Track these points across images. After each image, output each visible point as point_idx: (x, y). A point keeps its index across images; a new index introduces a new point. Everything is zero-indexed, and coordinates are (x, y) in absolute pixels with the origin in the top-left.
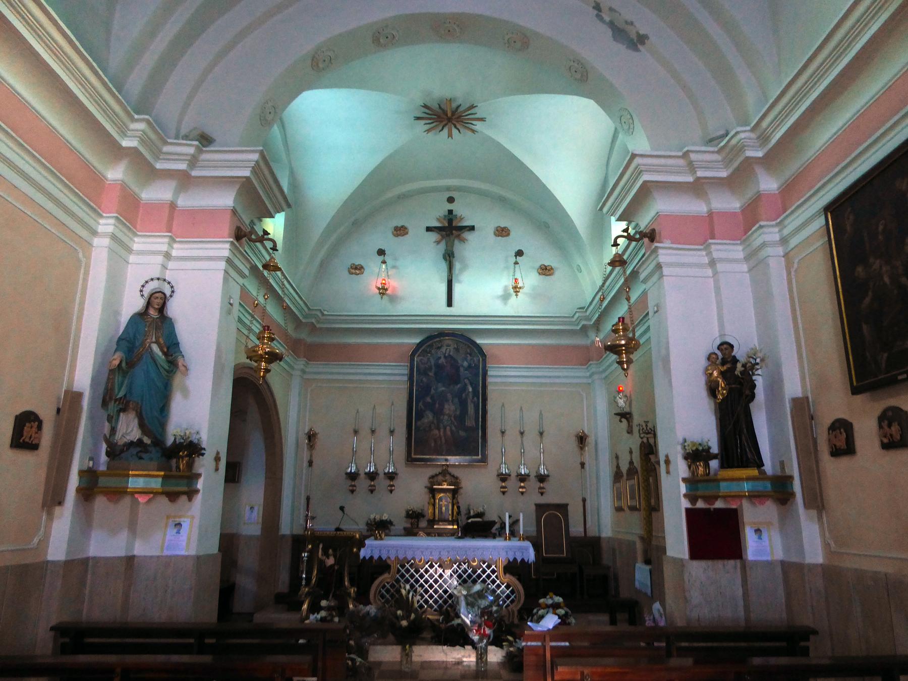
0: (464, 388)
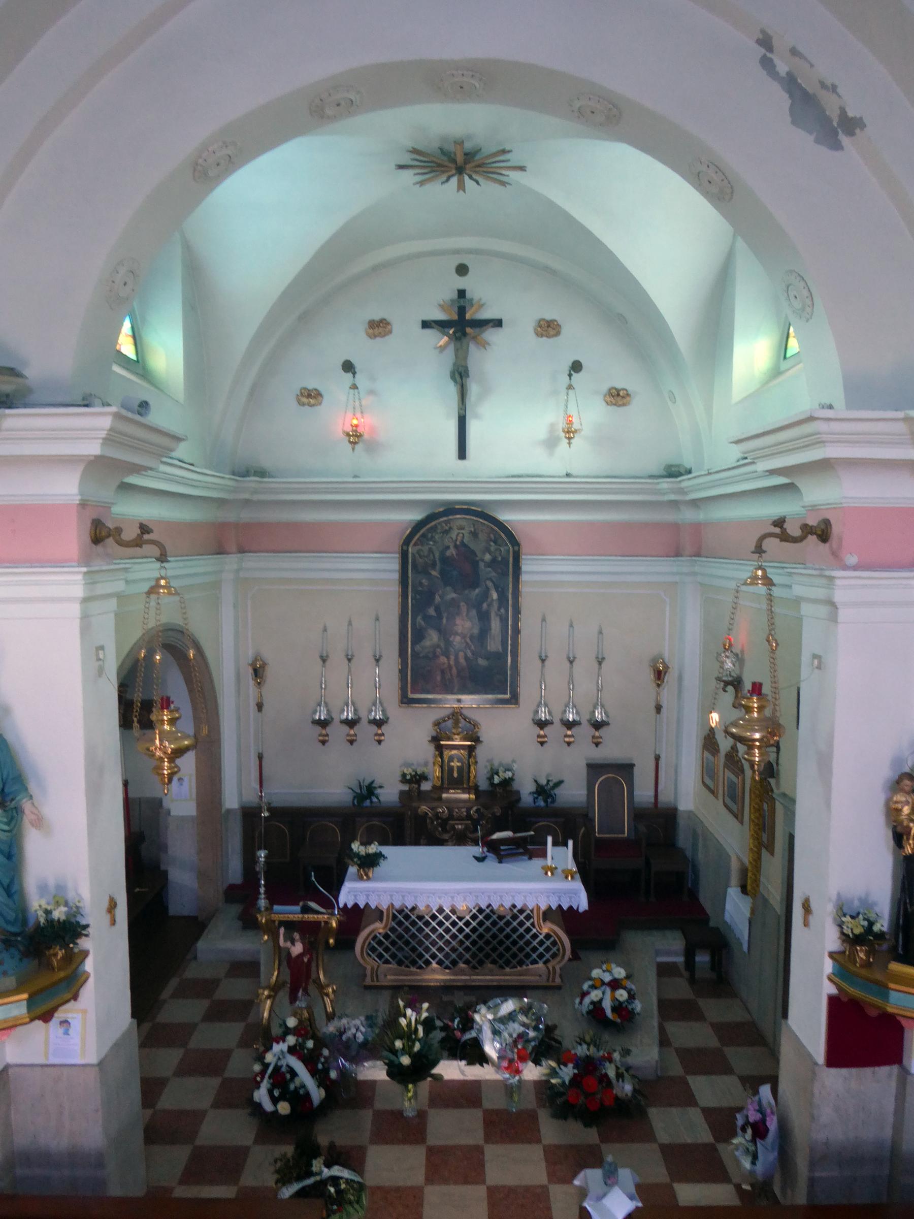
0: (486, 595)
